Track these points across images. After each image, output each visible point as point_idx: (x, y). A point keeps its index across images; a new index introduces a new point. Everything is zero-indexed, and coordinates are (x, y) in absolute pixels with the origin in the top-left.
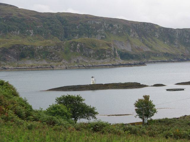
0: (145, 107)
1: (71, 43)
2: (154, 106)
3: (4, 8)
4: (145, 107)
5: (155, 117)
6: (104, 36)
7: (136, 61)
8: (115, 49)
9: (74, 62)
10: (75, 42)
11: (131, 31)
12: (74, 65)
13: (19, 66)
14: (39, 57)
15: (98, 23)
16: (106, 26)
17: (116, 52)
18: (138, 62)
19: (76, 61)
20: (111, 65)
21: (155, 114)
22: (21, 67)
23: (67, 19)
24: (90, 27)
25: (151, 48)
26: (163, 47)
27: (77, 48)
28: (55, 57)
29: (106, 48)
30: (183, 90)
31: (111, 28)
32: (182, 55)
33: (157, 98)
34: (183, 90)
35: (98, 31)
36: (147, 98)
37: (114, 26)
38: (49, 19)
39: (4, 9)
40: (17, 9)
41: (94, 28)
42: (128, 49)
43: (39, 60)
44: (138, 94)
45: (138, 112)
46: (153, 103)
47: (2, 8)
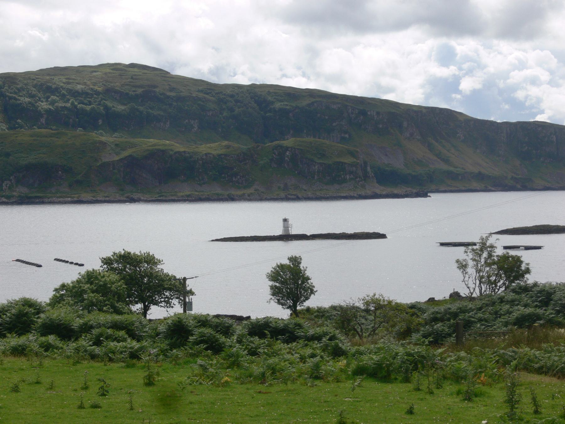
0: (290, 283)
1: (273, 150)
2: (309, 279)
3: (140, 73)
4: (290, 283)
5: (313, 302)
6: (347, 136)
7: (409, 189)
8: (365, 163)
9: (279, 188)
10: (281, 147)
11: (405, 124)
12: (278, 195)
13: (162, 196)
14: (206, 177)
15: (334, 107)
16: (352, 113)
17: (369, 169)
18: (415, 191)
19: (282, 186)
20: (355, 195)
21: (312, 295)
22: (166, 197)
23: (270, 98)
24: (319, 115)
25: (446, 161)
26: (472, 161)
27: (286, 159)
28: (239, 177)
29: (348, 160)
30: (539, 248)
31: (362, 117)
32: (512, 178)
33: (317, 262)
34: (539, 248)
35: (334, 124)
36: (296, 261)
37: (369, 113)
38: (232, 96)
39: (140, 75)
40: (168, 75)
41: (327, 118)
42: (397, 163)
43: (204, 183)
44: (281, 253)
45: (276, 292)
46: (308, 273)
47: (136, 73)
